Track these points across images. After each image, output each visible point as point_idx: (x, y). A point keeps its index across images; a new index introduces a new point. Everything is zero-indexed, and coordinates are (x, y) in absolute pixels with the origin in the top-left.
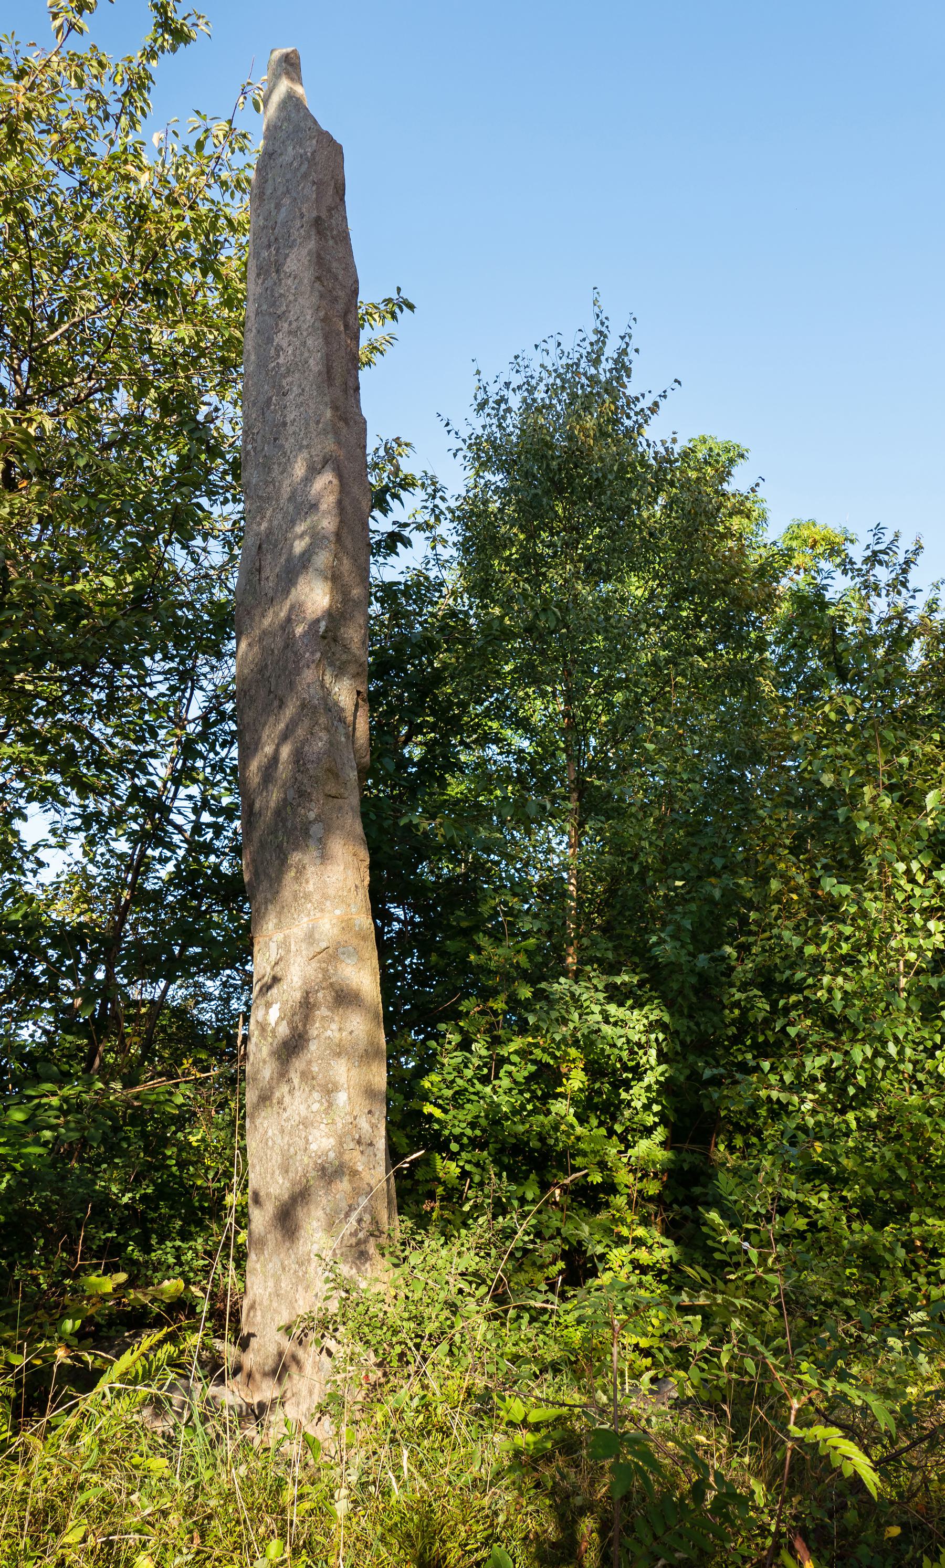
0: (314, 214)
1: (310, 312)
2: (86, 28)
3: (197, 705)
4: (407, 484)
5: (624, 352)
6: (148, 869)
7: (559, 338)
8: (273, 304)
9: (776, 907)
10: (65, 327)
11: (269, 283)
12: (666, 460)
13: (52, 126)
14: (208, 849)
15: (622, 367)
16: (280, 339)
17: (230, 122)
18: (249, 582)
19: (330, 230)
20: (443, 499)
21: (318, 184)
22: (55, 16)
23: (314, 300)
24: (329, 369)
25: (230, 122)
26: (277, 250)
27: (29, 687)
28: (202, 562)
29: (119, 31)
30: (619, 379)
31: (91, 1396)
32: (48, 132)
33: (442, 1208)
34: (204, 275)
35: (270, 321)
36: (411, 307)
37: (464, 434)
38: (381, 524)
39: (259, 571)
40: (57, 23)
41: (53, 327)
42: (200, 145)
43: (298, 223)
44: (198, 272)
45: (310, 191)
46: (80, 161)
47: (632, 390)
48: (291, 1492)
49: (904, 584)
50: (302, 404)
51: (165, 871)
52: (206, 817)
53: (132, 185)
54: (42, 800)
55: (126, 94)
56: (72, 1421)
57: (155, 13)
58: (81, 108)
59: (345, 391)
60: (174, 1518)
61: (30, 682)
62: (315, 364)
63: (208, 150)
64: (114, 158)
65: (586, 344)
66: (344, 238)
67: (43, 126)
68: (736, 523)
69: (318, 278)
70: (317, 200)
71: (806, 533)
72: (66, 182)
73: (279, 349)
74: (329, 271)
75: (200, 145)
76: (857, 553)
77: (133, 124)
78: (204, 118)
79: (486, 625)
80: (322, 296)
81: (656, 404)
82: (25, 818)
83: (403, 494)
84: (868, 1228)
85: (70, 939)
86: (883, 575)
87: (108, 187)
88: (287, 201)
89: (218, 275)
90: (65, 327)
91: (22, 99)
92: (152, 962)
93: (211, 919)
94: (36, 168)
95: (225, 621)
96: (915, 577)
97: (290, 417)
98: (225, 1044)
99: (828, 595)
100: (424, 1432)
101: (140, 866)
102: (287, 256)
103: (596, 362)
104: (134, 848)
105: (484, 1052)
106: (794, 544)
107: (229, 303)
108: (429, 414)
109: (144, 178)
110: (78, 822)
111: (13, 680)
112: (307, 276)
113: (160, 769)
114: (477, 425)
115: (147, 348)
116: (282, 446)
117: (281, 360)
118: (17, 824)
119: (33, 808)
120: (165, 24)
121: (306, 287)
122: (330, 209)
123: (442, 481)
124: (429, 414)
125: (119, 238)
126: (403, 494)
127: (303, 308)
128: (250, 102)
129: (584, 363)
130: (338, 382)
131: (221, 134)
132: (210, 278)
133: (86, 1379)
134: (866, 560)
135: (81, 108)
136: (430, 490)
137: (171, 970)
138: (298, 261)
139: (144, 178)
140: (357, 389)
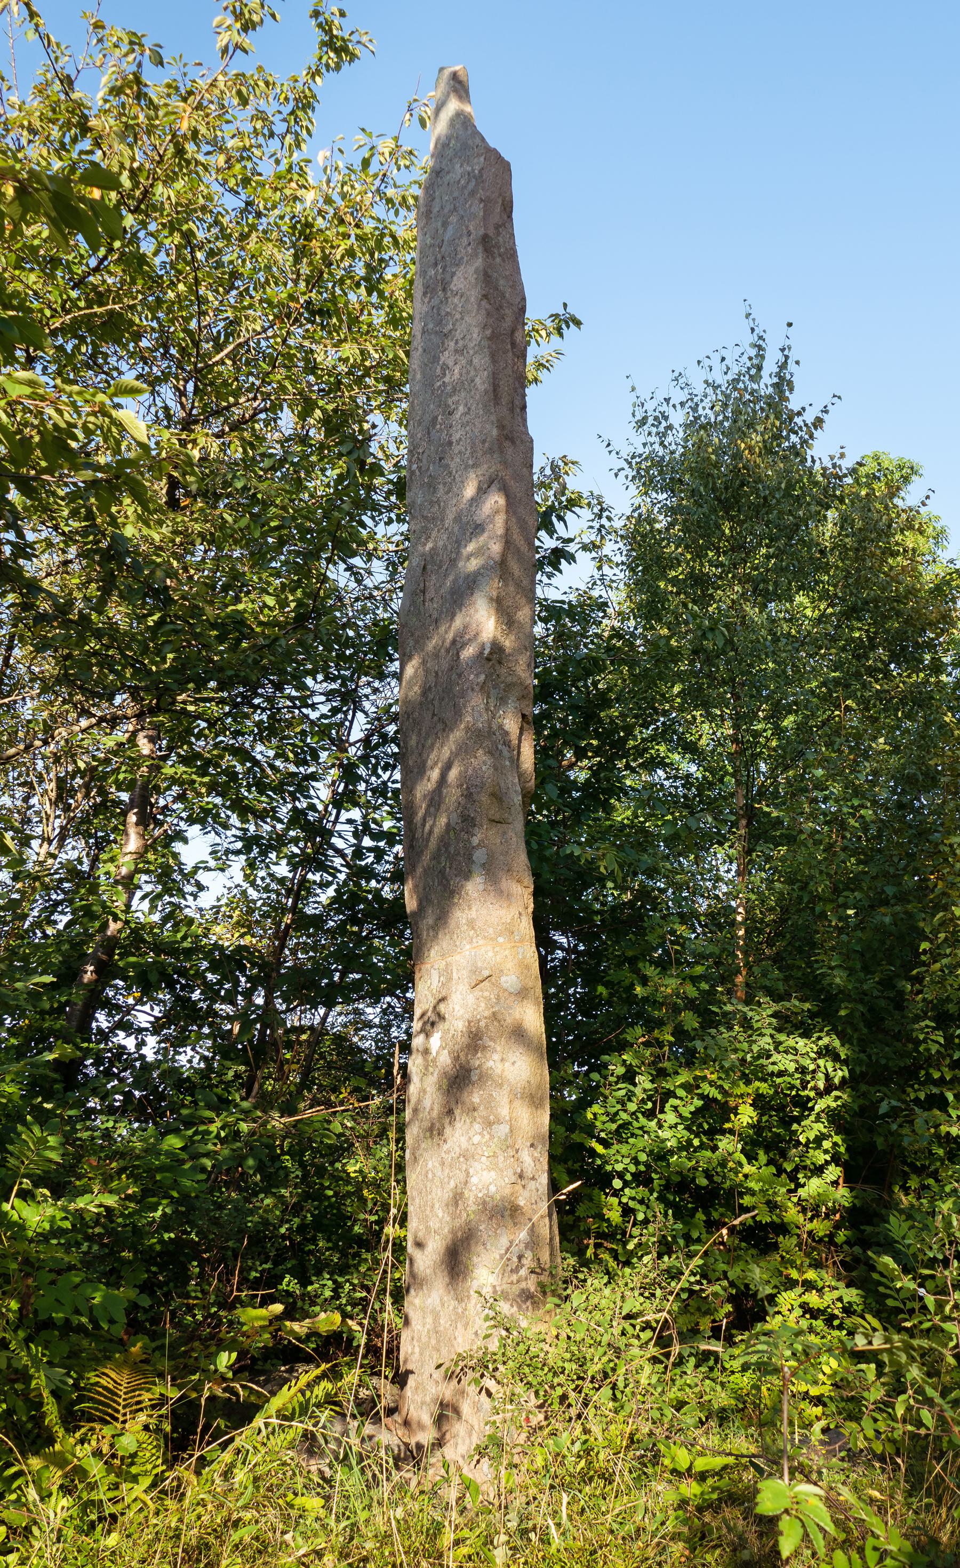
0: (482, 232)
1: (476, 330)
3: (358, 729)
5: (783, 366)
6: (310, 893)
7: (724, 353)
8: (439, 323)
11: (435, 302)
14: (368, 873)
15: (783, 384)
16: (446, 358)
17: (396, 139)
18: (413, 603)
19: (497, 247)
21: (485, 201)
23: (481, 318)
24: (495, 388)
25: (396, 139)
28: (363, 581)
29: (286, 51)
36: (578, 323)
39: (424, 592)
41: (219, 347)
42: (366, 163)
43: (465, 241)
45: (477, 209)
48: (448, 1537)
50: (468, 422)
52: (367, 842)
59: (512, 410)
62: (481, 382)
63: (374, 168)
65: (745, 359)
66: (512, 255)
69: (485, 296)
70: (485, 218)
72: (232, 203)
73: (445, 368)
75: (366, 163)
78: (370, 135)
82: (185, 841)
85: (229, 962)
88: (454, 219)
92: (308, 987)
93: (374, 944)
97: (456, 437)
101: (301, 890)
102: (453, 274)
103: (755, 378)
109: (309, 196)
110: (239, 845)
112: (474, 294)
113: (322, 792)
114: (636, 442)
116: (447, 466)
117: (447, 379)
118: (178, 846)
119: (193, 831)
122: (497, 227)
123: (608, 501)
125: (285, 257)
127: (470, 325)
128: (416, 119)
131: (387, 151)
133: (242, 1414)
136: (596, 510)
138: (465, 280)
140: (524, 407)
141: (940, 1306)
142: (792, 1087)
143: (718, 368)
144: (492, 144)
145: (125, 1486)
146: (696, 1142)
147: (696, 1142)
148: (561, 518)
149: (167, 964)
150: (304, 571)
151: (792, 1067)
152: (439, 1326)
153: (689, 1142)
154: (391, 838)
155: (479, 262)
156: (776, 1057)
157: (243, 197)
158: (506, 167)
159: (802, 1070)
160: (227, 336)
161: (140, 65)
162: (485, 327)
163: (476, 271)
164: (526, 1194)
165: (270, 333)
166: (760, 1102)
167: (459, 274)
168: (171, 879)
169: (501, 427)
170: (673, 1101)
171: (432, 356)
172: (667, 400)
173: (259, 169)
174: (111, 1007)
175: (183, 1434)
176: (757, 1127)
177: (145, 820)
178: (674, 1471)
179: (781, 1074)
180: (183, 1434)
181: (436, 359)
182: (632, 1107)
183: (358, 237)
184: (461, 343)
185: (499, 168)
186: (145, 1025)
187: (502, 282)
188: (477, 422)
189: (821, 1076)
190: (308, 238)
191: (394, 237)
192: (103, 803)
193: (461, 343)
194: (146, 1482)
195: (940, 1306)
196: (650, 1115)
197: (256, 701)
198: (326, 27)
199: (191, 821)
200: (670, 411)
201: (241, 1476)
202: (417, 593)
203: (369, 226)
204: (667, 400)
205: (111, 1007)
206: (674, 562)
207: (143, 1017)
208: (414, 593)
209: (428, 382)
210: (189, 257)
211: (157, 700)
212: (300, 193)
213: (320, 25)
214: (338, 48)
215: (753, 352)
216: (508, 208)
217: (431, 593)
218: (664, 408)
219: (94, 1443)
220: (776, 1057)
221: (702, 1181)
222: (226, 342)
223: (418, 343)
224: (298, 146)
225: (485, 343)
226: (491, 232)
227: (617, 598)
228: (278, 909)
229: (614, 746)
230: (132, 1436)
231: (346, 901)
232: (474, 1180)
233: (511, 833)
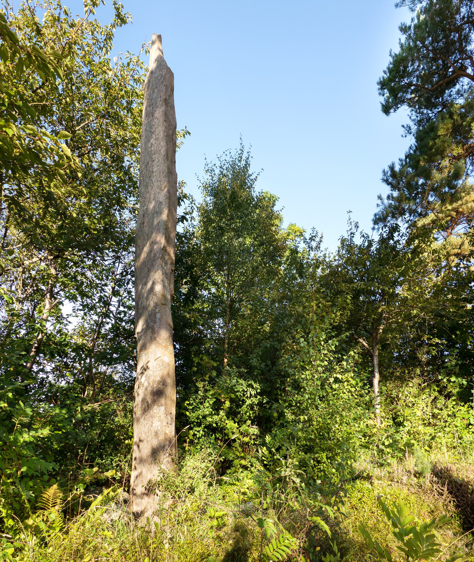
0: (164, 97)
1: (162, 132)
2: (95, 13)
3: (119, 269)
4: (185, 196)
5: (248, 159)
6: (104, 326)
7: (230, 151)
8: (150, 128)
9: (283, 351)
10: (82, 125)
11: (149, 120)
12: (260, 200)
13: (82, 48)
14: (121, 320)
15: (247, 165)
16: (152, 141)
17: (138, 57)
18: (140, 227)
19: (169, 103)
20: (194, 204)
21: (166, 86)
22: (86, 6)
23: (163, 128)
24: (167, 154)
25: (138, 57)
26: (153, 108)
27: (69, 257)
28: (126, 219)
29: (105, 16)
30: (247, 167)
31: (89, 511)
32: (80, 49)
33: (189, 446)
34: (128, 113)
35: (149, 134)
36: (189, 133)
37: (202, 182)
38: (180, 211)
39: (143, 223)
40: (87, 8)
41: (78, 124)
42: (128, 64)
43: (159, 99)
44: (126, 111)
45: (163, 88)
46: (89, 62)
47: (250, 172)
48: (150, 541)
49: (319, 248)
50: (159, 166)
51: (108, 327)
52: (122, 309)
53: (106, 75)
54: (70, 300)
55: (105, 40)
56: (82, 519)
57: (115, 11)
58: (91, 42)
59: (172, 163)
60: (116, 551)
61: (69, 256)
62: (163, 151)
63: (131, 66)
64: (100, 63)
65: (237, 154)
66: (173, 107)
67: (79, 47)
68: (277, 222)
69: (165, 121)
70: (166, 92)
71: (293, 228)
72: (86, 70)
73: (152, 144)
74: (168, 118)
75: (128, 64)
76: (308, 236)
77: (107, 51)
78: (130, 54)
79: (206, 249)
80: (166, 127)
81: (256, 177)
82: (63, 305)
83: (185, 200)
84: (303, 453)
85: (78, 349)
86: (314, 244)
87: (99, 75)
88: (156, 91)
89: (132, 114)
90: (82, 125)
91: (74, 36)
92: (104, 358)
93: (123, 345)
94: (76, 63)
95: (131, 240)
96: (322, 246)
97: (154, 170)
98: (128, 389)
99: (299, 249)
100: (186, 520)
101: (100, 325)
102: (155, 111)
103: (240, 161)
104: (99, 318)
105: (202, 394)
106: (290, 231)
107: (135, 124)
108: (195, 174)
109: (110, 73)
110: (81, 308)
111: (64, 254)
112: (162, 119)
113: (108, 289)
114: (206, 178)
115: (109, 136)
116: (152, 180)
117: (152, 149)
118: (61, 307)
119: (66, 302)
120: (118, 16)
121: (161, 123)
122: (169, 96)
123: (195, 198)
124: (195, 174)
125: (101, 94)
126: (185, 200)
127: (160, 131)
128: (144, 50)
129: (237, 161)
130: (170, 159)
131: (135, 61)
132: (130, 115)
133: (86, 505)
134: (310, 239)
135: (91, 42)
136: (191, 200)
137: (111, 362)
138: (159, 113)
139: (110, 73)
140: (175, 162)
141: (286, 463)
142: (240, 396)
143: (229, 155)
144: (169, 66)
145: (51, 531)
146: (213, 413)
147: (213, 413)
148: (183, 200)
149: (53, 347)
150: (106, 213)
151: (241, 390)
152: (144, 474)
153: (212, 412)
154: (129, 308)
156: (237, 386)
157: (89, 68)
159: (243, 391)
160: (81, 120)
161: (59, 14)
162: (164, 132)
163: (163, 111)
164: (169, 429)
165: (95, 122)
166: (232, 401)
167: (157, 111)
168: (59, 319)
169: (168, 168)
170: (208, 399)
171: (148, 139)
172: (215, 165)
173: (94, 59)
174: (39, 364)
175: (70, 512)
176: (230, 408)
177: (52, 296)
178: (210, 517)
179: (238, 391)
180: (70, 512)
182: (197, 401)
183: (125, 92)
185: (171, 74)
186: (49, 370)
188: (161, 165)
189: (249, 393)
190: (110, 89)
191: (136, 93)
192: (37, 290)
194: (58, 529)
195: (286, 463)
196: (201, 403)
197: (90, 256)
198: (117, 9)
199: (67, 297)
200: (215, 169)
201: (88, 525)
202: (141, 225)
203: (129, 88)
204: (215, 165)
205: (39, 364)
206: (213, 221)
207: (48, 368)
208: (141, 224)
209: (146, 149)
210: (70, 88)
211: (58, 254)
212: (108, 71)
213: (115, 8)
214: (121, 19)
215: (240, 152)
217: (146, 224)
218: (213, 167)
219: (41, 517)
220: (237, 386)
221: (214, 425)
222: (81, 122)
223: (143, 134)
224: (107, 53)
225: (164, 138)
226: (167, 98)
227: (198, 232)
228: (93, 331)
229: (195, 282)
230: (54, 514)
231: (115, 329)
232: (154, 425)
233: (167, 309)
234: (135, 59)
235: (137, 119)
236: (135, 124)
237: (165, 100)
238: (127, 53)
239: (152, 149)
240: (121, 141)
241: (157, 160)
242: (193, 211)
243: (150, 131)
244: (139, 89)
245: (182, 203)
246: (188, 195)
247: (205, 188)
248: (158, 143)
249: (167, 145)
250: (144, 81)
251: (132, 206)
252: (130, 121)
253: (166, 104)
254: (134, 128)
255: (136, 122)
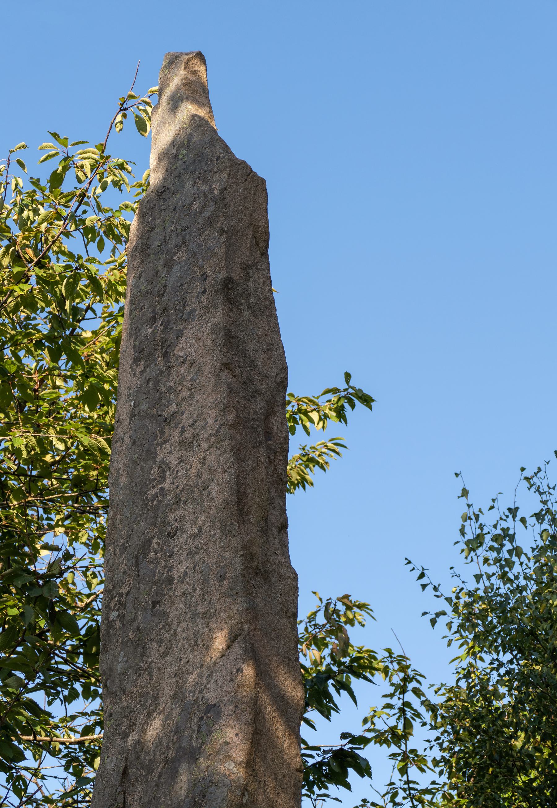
0: (223, 274)
1: (213, 414)
8: (157, 402)
16: (167, 453)
19: (245, 296)
20: (417, 692)
21: (230, 233)
23: (220, 396)
25: (102, 147)
26: (166, 325)
34: (55, 357)
36: (367, 400)
37: (449, 590)
42: (56, 179)
43: (198, 287)
45: (217, 243)
59: (265, 531)
62: (219, 490)
66: (266, 308)
69: (227, 365)
73: (164, 467)
78: (64, 142)
80: (231, 391)
83: (356, 683)
88: (182, 257)
102: (180, 333)
107: (89, 398)
112: (210, 363)
114: (464, 573)
116: (165, 614)
117: (167, 485)
122: (246, 268)
123: (416, 664)
126: (356, 683)
127: (203, 405)
130: (254, 516)
131: (87, 164)
138: (197, 341)
140: (284, 527)
144: (239, 155)
155: (218, 317)
158: (260, 185)
167: (188, 334)
169: (248, 556)
172: (513, 511)
181: (151, 455)
184: (189, 432)
187: (251, 345)
193: (189, 432)
204: (513, 511)
216: (261, 241)
218: (509, 523)
225: (226, 432)
226: (237, 275)
234: (84, 158)
235: (102, 379)
236: (89, 398)
237: (228, 287)
238: (50, 143)
239: (167, 485)
240: (20, 473)
241: (190, 529)
242: (408, 725)
243: (155, 415)
244: (108, 263)
245: (341, 699)
246: (381, 654)
247: (469, 620)
248: (199, 463)
249: (239, 458)
250: (127, 228)
251: (75, 737)
252: (67, 391)
253: (228, 300)
254: (85, 412)
255: (95, 389)
